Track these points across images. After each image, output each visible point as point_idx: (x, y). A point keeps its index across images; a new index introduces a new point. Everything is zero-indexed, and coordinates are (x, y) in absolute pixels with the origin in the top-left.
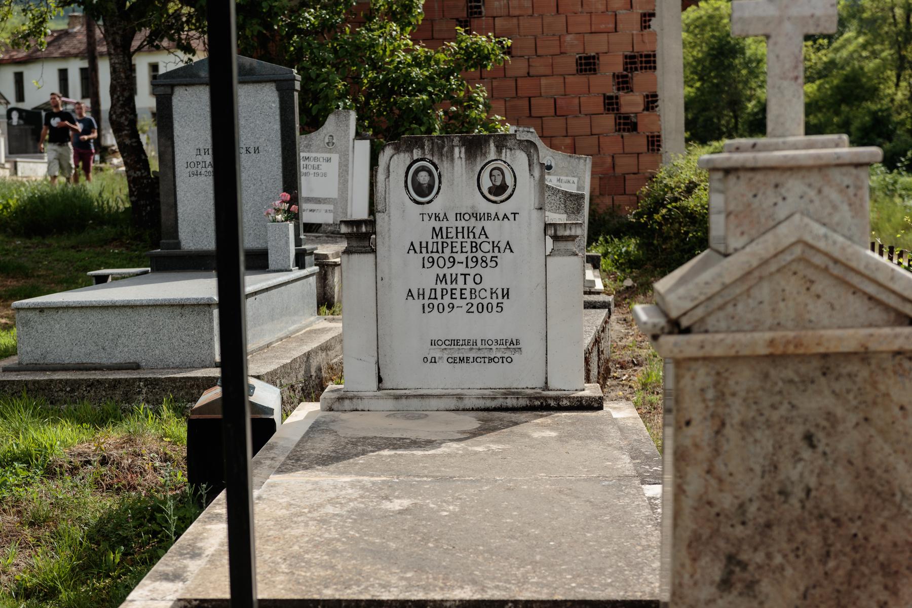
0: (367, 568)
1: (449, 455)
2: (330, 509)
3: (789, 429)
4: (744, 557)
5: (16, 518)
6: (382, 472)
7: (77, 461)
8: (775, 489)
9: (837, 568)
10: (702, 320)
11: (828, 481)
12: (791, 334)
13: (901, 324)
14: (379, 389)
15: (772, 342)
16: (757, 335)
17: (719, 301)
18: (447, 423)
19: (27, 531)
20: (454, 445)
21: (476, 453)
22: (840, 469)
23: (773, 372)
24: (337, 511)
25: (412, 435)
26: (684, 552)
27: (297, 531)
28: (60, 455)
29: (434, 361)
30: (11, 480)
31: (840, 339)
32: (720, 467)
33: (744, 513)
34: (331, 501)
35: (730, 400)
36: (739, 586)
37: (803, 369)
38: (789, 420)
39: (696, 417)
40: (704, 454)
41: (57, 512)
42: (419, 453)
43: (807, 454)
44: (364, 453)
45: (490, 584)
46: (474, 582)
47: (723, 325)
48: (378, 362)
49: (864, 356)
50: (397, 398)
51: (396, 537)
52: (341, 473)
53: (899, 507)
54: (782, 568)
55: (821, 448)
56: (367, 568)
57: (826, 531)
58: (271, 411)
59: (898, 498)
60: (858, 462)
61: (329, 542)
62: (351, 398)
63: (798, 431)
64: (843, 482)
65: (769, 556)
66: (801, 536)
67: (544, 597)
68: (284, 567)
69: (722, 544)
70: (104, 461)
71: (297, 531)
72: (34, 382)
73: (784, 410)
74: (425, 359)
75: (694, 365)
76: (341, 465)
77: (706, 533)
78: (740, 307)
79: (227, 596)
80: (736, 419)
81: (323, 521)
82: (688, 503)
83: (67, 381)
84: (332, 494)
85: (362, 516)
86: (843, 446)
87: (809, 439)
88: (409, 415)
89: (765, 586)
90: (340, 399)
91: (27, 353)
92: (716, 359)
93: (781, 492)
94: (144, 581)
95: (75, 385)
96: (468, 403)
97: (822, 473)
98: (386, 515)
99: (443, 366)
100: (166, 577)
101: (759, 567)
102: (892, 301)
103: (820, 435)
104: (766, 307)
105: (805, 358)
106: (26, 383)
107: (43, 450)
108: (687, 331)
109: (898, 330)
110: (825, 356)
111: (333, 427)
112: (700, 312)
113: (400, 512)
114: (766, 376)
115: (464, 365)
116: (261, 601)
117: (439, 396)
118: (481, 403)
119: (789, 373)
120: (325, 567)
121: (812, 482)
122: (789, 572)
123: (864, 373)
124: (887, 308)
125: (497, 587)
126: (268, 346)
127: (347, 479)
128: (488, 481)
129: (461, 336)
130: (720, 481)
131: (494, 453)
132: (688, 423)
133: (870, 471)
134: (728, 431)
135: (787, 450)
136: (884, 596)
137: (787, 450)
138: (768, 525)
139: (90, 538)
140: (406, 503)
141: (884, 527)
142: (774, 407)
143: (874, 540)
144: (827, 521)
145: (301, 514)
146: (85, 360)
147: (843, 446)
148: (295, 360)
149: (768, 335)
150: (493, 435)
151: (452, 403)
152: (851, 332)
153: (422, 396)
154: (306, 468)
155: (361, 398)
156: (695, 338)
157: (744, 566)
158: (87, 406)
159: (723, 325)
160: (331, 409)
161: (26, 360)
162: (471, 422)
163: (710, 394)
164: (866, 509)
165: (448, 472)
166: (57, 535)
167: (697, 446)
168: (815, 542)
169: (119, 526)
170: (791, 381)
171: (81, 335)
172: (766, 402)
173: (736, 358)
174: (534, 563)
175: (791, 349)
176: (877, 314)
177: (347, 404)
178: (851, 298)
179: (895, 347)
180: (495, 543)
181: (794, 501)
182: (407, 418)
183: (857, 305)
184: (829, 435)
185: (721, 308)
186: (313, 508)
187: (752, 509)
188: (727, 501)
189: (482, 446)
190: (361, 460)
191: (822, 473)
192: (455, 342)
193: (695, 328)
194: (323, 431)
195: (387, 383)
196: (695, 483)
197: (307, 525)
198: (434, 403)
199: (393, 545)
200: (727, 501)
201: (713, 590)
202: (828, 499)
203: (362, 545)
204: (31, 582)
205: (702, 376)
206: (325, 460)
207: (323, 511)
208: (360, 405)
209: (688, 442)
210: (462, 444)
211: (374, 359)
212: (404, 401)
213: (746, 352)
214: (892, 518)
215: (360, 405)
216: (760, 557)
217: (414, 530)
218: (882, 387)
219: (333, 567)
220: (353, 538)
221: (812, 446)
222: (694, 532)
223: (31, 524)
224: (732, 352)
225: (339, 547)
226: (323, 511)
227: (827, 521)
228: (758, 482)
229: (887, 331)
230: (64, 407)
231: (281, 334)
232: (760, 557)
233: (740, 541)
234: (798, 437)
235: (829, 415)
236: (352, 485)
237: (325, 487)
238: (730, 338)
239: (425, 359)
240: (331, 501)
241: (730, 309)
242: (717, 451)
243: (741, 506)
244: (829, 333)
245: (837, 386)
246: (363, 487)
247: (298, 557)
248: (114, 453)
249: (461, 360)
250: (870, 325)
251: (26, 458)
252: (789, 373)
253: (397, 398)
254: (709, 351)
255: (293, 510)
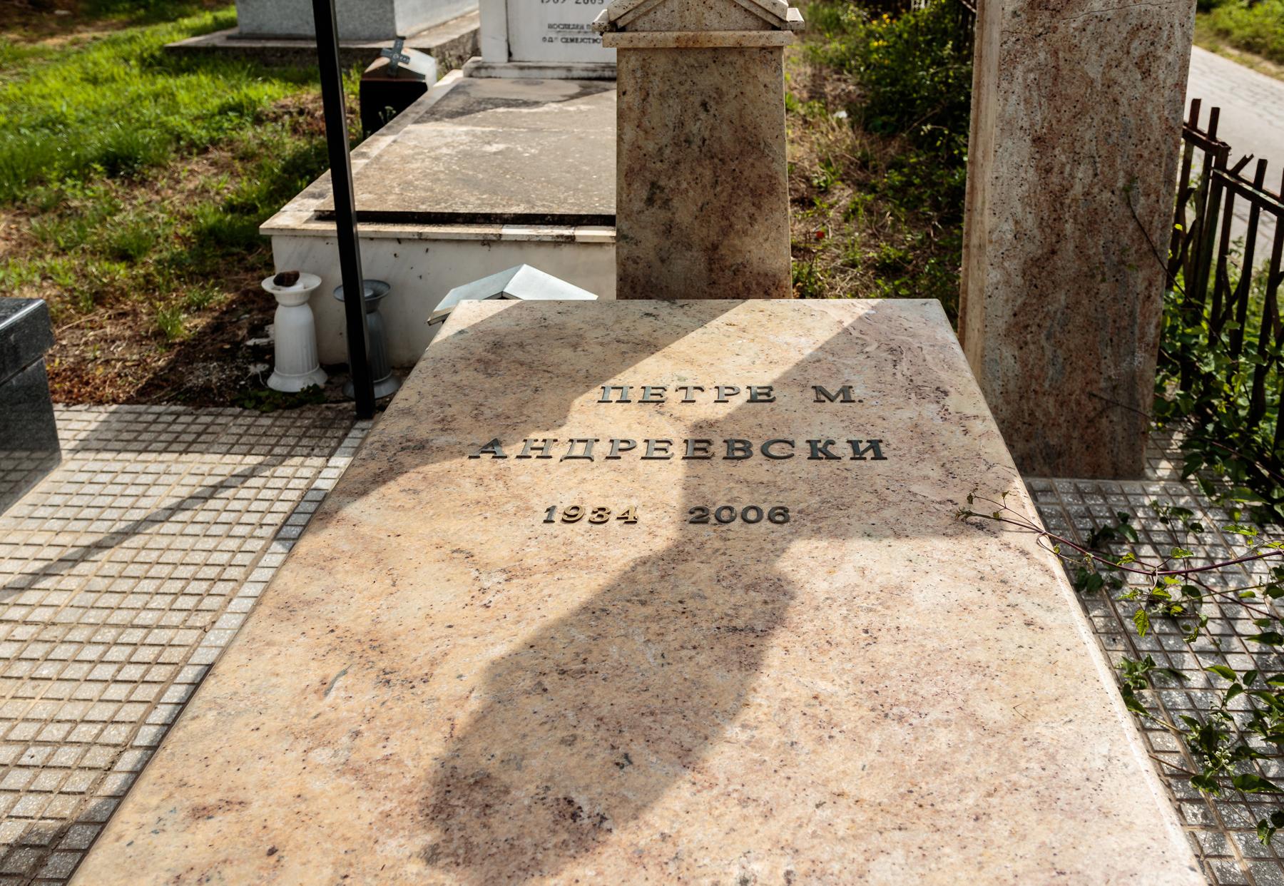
0: (456, 192)
1: (547, 113)
2: (445, 151)
3: (691, 99)
4: (662, 183)
5: (230, 154)
6: (492, 124)
7: (280, 111)
8: (682, 139)
9: (722, 191)
10: (633, 22)
11: (717, 134)
12: (691, 34)
13: (766, 29)
14: (509, 61)
15: (678, 39)
16: (668, 34)
17: (643, 9)
18: (556, 88)
19: (237, 164)
20: (554, 105)
21: (568, 112)
22: (724, 126)
23: (680, 60)
24: (449, 152)
25: (524, 97)
26: (623, 180)
27: (415, 166)
28: (267, 106)
29: (551, 40)
30: (226, 125)
31: (724, 38)
32: (646, 123)
33: (662, 154)
34: (447, 145)
35: (652, 78)
36: (659, 202)
37: (701, 58)
38: (691, 93)
39: (630, 89)
40: (635, 114)
41: (263, 150)
42: (525, 110)
43: (703, 116)
44: (484, 109)
45: (539, 203)
46: (528, 202)
47: (647, 26)
48: (508, 41)
49: (739, 50)
50: (522, 68)
51: (486, 171)
52: (462, 124)
53: (763, 152)
54: (687, 191)
55: (712, 112)
56: (456, 192)
57: (715, 168)
58: (423, 77)
59: (762, 145)
60: (737, 122)
61: (435, 173)
62: (486, 68)
63: (696, 100)
64: (726, 134)
65: (678, 183)
66: (699, 170)
67: (573, 212)
68: (397, 190)
69: (647, 174)
70: (301, 112)
71: (415, 166)
72: (252, 49)
73: (687, 86)
74: (544, 39)
75: (628, 54)
76: (463, 118)
77: (637, 167)
78: (659, 14)
79: (333, 208)
80: (657, 91)
81: (437, 159)
82: (626, 147)
83: (277, 49)
84: (449, 140)
85: (466, 155)
86: (726, 111)
87: (704, 105)
88: (529, 82)
89: (676, 202)
90: (478, 68)
91: (246, 25)
92: (643, 49)
93: (686, 141)
94: (297, 198)
95: (284, 51)
96: (575, 74)
97: (713, 129)
98: (483, 155)
99: (558, 45)
100: (313, 196)
101: (672, 190)
102: (759, 12)
103: (712, 103)
104: (676, 14)
105: (702, 50)
106: (245, 49)
107: (253, 103)
108: (623, 29)
109: (762, 33)
110: (715, 49)
111: (468, 90)
112: (630, 17)
113: (495, 153)
114: (676, 62)
115: (574, 44)
116: (359, 212)
117: (553, 68)
118: (585, 74)
119: (691, 61)
120: (426, 190)
121: (707, 134)
122: (691, 193)
123: (741, 62)
124: (757, 17)
125: (543, 206)
126: (444, 24)
127: (464, 129)
128: (567, 132)
129: (571, 21)
130: (646, 132)
131: (581, 112)
132: (624, 93)
133: (744, 129)
134: (651, 99)
135: (690, 113)
136: (752, 210)
137: (690, 113)
138: (678, 163)
139: (284, 170)
140: (501, 146)
141: (753, 165)
142: (681, 83)
143: (746, 173)
144: (716, 160)
145: (422, 153)
146: (293, 32)
147: (726, 111)
148: (462, 36)
149: (676, 34)
150: (586, 99)
151: (564, 74)
152: (731, 33)
153: (540, 68)
154: (437, 120)
155: (493, 68)
156: (627, 35)
157: (662, 189)
158: (294, 69)
159: (647, 26)
160: (471, 76)
161: (246, 30)
162: (574, 88)
163: (639, 74)
164: (741, 153)
165: (540, 124)
166: (260, 167)
167: (630, 108)
168: (708, 173)
169: (306, 161)
170: (693, 66)
171: (288, 11)
172: (676, 80)
173: (655, 49)
174: (576, 190)
175: (691, 44)
176: (750, 22)
177: (483, 72)
178: (733, 9)
179: (760, 44)
180: (554, 175)
181: (695, 147)
182: (527, 84)
183: (736, 15)
184: (717, 103)
185: (646, 14)
186: (432, 149)
187: (667, 151)
188: (650, 147)
189: (581, 105)
190: (480, 115)
191: (713, 129)
192: (567, 26)
193: (629, 28)
194: (459, 93)
195: (515, 57)
196: (630, 134)
197: (423, 161)
198: (549, 73)
199: (480, 176)
200: (650, 147)
201: (642, 204)
202: (716, 146)
203: (459, 176)
204: (238, 201)
205: (634, 61)
206: (453, 115)
207: (438, 152)
208: (493, 73)
209: (624, 106)
210: (560, 105)
211: (504, 38)
212: (526, 72)
213: (660, 45)
214: (758, 159)
215: (493, 73)
216: (672, 183)
217: (500, 166)
218: (752, 72)
219: (432, 190)
220: (454, 171)
221: (707, 111)
222: (629, 166)
223: (242, 159)
224: (652, 46)
225: (442, 176)
226: (438, 152)
227: (716, 160)
228: (671, 133)
229: (755, 33)
230: (276, 69)
231: (456, 14)
232: (672, 183)
233: (660, 173)
234: (697, 104)
235: (718, 89)
236: (467, 133)
237: (446, 133)
238: (650, 35)
239: (544, 39)
240: (447, 145)
241: (652, 15)
242: (644, 113)
243: (660, 149)
244: (717, 33)
245: (723, 70)
246: (475, 135)
247: (409, 183)
248: (310, 106)
249: (572, 40)
250: (746, 29)
251: (238, 108)
252: (691, 61)
253: (522, 68)
254: (636, 44)
255: (417, 150)
